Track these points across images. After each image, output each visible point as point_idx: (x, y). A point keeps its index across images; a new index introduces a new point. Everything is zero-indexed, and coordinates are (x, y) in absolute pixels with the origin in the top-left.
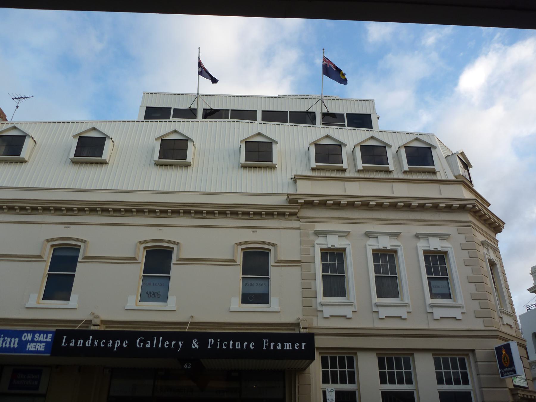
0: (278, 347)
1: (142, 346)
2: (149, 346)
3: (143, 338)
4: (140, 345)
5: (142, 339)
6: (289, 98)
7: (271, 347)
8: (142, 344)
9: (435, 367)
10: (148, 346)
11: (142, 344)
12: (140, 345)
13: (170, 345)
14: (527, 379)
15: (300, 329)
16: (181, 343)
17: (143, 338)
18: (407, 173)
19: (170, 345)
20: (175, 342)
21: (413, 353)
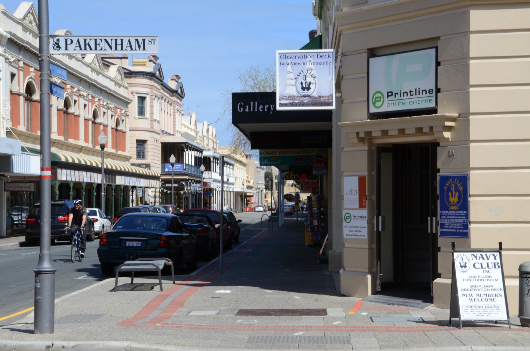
0: (246, 110)
1: (242, 111)
2: (248, 111)
3: (242, 103)
4: (240, 110)
5: (241, 104)
6: (354, 230)
7: (265, 110)
8: (242, 109)
9: (291, 291)
10: (247, 110)
11: (242, 109)
12: (240, 110)
13: (264, 109)
14: (151, 75)
15: (50, 253)
16: (272, 106)
17: (242, 103)
18: (20, 50)
19: (264, 109)
20: (267, 106)
21: (335, 48)
